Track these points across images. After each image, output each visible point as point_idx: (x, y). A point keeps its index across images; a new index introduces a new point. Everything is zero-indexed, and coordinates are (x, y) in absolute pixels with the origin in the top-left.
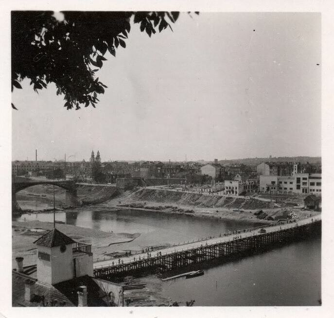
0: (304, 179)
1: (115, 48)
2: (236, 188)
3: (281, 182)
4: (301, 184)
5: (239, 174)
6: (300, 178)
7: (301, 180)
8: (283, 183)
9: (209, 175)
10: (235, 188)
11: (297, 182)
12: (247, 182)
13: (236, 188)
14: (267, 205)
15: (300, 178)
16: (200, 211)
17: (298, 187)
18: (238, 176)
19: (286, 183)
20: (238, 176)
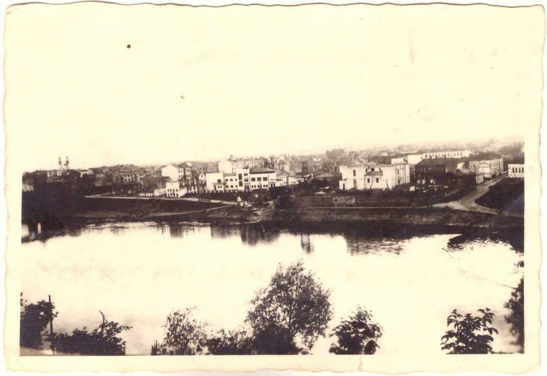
0: (246, 175)
1: (58, 334)
2: (177, 190)
3: (227, 180)
4: (243, 181)
5: (112, 328)
6: (241, 174)
7: (243, 175)
8: (229, 180)
9: (124, 165)
10: (175, 190)
11: (239, 179)
12: (73, 187)
13: (177, 190)
14: (187, 195)
15: (241, 174)
16: (111, 220)
17: (241, 184)
18: (202, 176)
19: (231, 180)
20: (202, 176)
